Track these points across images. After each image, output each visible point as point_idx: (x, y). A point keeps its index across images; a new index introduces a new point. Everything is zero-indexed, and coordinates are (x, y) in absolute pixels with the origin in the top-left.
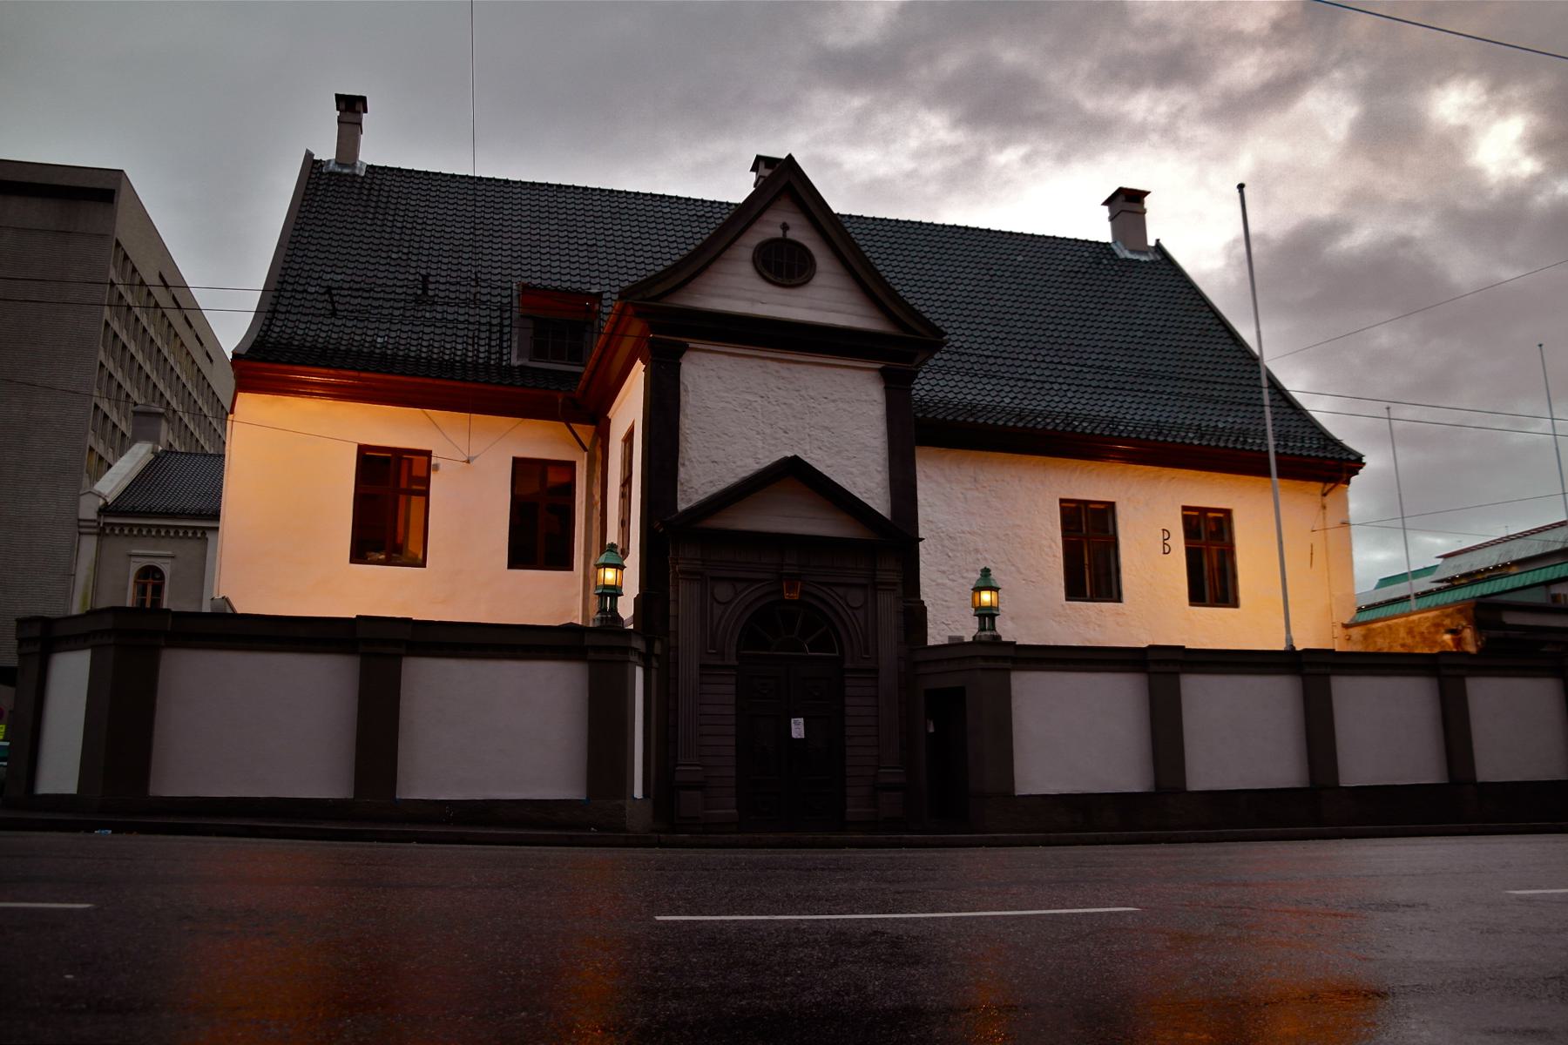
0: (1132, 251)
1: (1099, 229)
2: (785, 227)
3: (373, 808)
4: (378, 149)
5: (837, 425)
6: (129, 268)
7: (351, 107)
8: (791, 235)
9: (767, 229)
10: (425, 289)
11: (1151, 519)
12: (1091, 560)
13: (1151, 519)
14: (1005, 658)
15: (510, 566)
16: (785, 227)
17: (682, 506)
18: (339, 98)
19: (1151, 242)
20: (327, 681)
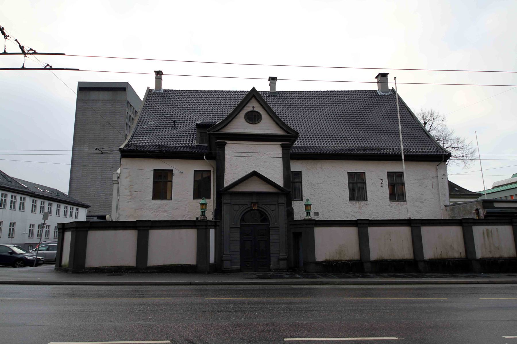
0: (383, 92)
1: (374, 87)
2: (253, 107)
3: (141, 267)
4: (167, 85)
5: (269, 161)
6: (132, 108)
7: (159, 74)
8: (255, 109)
9: (248, 108)
10: (175, 125)
11: (376, 176)
12: (357, 189)
13: (376, 176)
14: (312, 224)
15: (194, 198)
16: (253, 107)
17: (225, 185)
18: (155, 72)
19: (390, 88)
20: (130, 237)
